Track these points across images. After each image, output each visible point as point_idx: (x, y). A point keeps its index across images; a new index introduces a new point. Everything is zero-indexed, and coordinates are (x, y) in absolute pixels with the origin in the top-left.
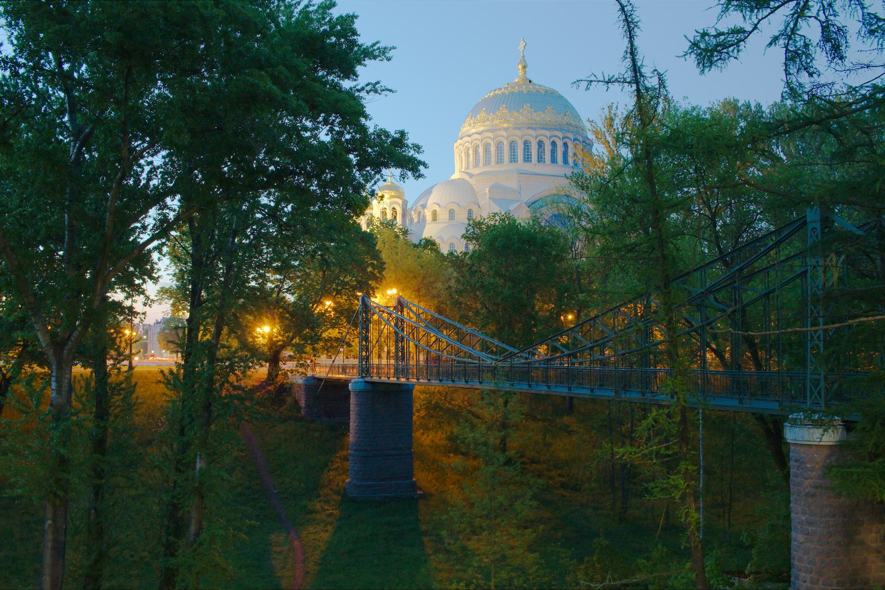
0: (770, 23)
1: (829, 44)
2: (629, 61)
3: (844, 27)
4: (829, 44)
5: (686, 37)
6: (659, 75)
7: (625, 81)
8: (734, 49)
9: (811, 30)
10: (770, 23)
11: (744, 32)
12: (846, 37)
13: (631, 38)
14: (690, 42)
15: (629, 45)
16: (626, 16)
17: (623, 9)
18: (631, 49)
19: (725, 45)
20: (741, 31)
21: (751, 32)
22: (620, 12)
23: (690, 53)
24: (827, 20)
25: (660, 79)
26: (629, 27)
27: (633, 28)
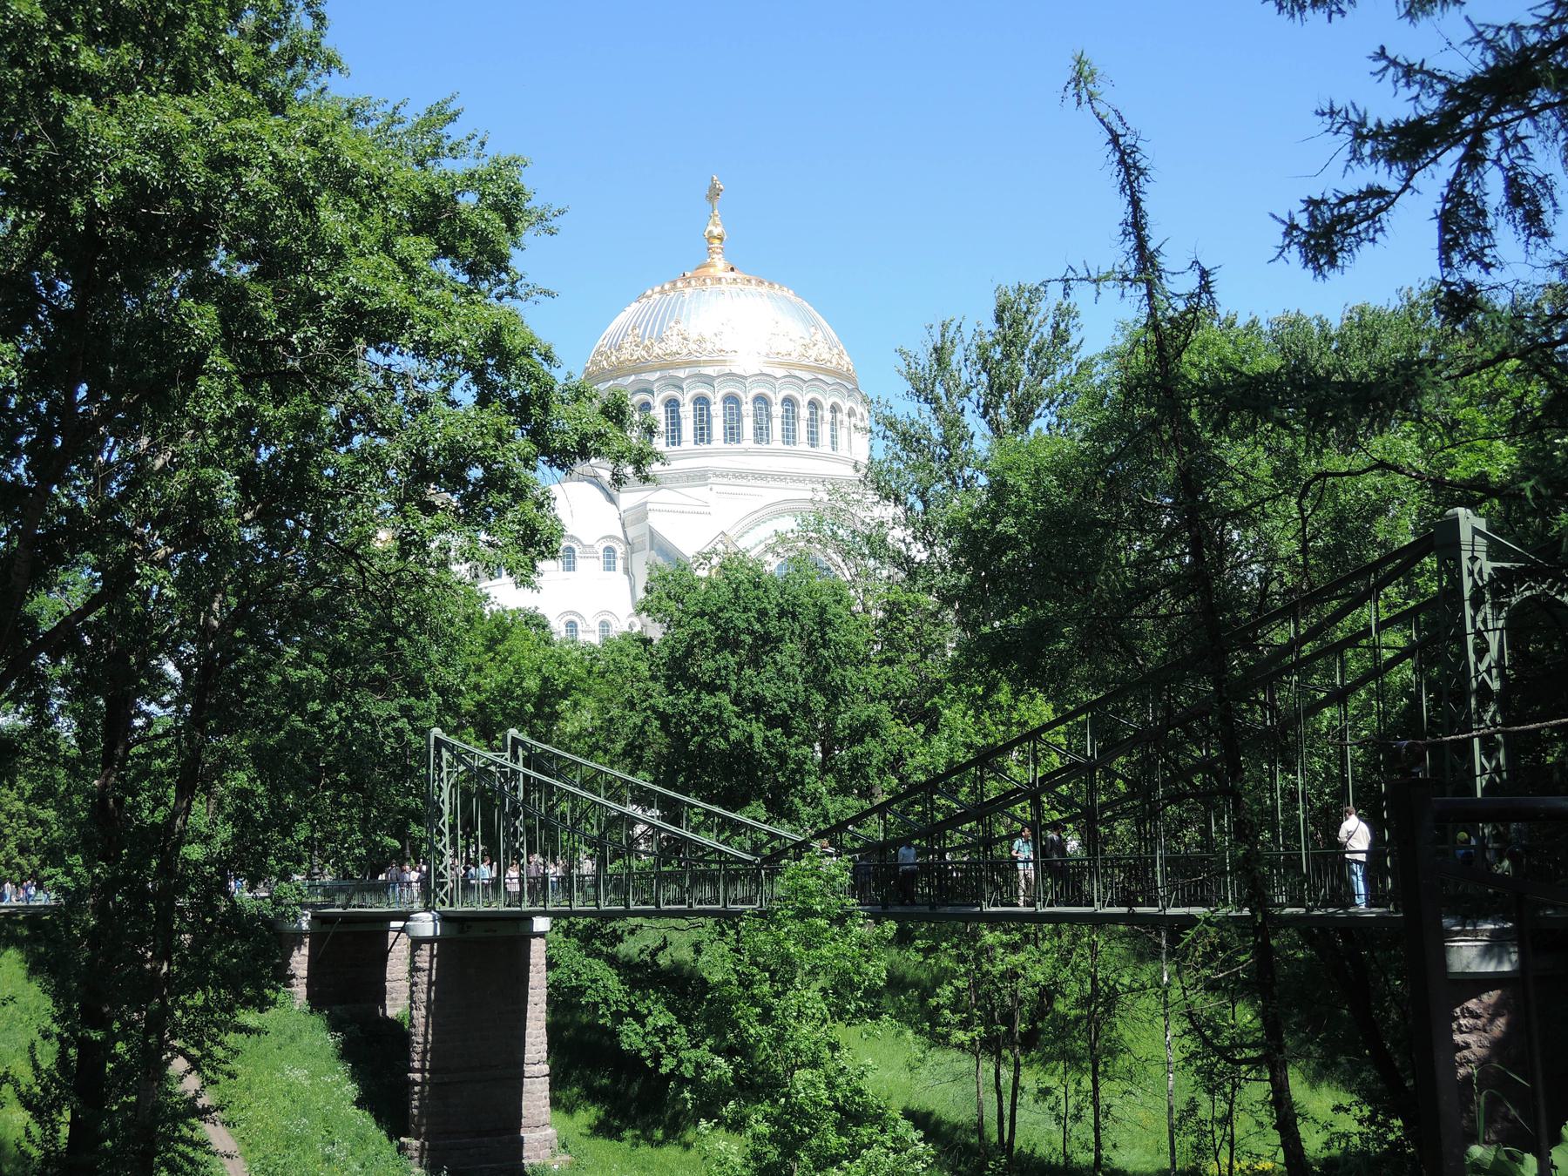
0: (1433, 177)
1: (1519, 212)
2: (1131, 243)
3: (1546, 176)
4: (1519, 212)
5: (1274, 216)
6: (1204, 274)
7: (1125, 278)
8: (1369, 226)
9: (1493, 187)
10: (1433, 177)
11: (1387, 193)
12: (1552, 196)
13: (1136, 225)
14: (1283, 222)
15: (1130, 210)
16: (1123, 153)
17: (1115, 139)
18: (1134, 217)
19: (1350, 220)
20: (1380, 193)
21: (1398, 195)
22: (1111, 146)
23: (1288, 246)
24: (1513, 167)
25: (1202, 277)
26: (1128, 174)
27: (1137, 178)
